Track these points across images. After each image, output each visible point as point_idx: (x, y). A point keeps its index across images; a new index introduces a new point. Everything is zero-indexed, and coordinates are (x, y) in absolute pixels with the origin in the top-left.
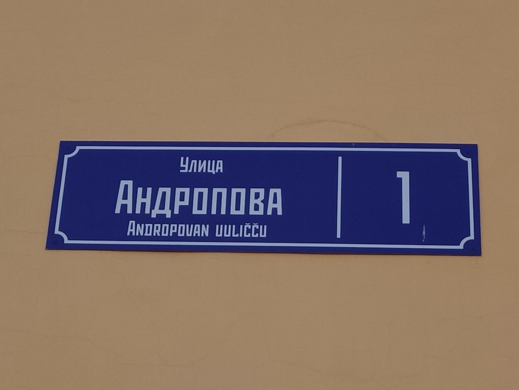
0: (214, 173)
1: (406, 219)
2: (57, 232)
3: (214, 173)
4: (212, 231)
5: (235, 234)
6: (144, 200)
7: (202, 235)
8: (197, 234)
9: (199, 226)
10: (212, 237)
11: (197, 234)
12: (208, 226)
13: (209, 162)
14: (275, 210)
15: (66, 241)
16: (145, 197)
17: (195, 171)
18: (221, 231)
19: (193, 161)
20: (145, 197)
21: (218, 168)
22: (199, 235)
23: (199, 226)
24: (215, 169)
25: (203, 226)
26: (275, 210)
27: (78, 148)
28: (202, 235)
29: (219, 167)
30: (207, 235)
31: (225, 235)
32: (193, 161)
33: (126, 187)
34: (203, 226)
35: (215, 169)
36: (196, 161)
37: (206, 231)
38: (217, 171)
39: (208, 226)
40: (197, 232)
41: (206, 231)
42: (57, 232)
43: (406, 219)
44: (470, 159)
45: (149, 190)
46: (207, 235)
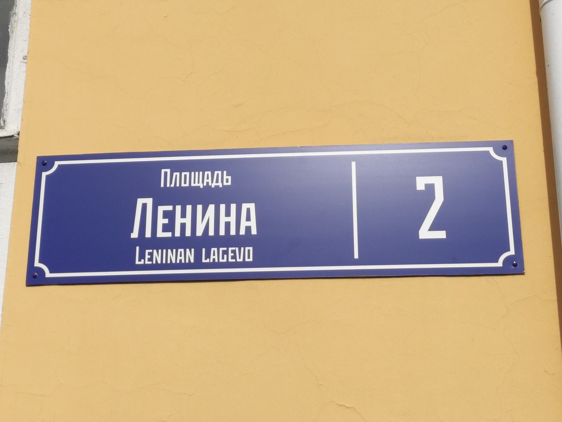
0: (202, 187)
1: (138, 248)
2: (37, 264)
3: (202, 187)
4: (198, 256)
5: (206, 259)
6: (183, 220)
7: (187, 261)
8: (181, 260)
9: (182, 250)
10: (198, 264)
11: (181, 260)
12: (193, 250)
13: (197, 173)
14: (248, 229)
15: (48, 275)
16: (185, 217)
17: (178, 185)
18: (216, 254)
19: (175, 174)
20: (185, 217)
21: (206, 181)
22: (183, 261)
23: (182, 250)
24: (203, 182)
25: (188, 250)
26: (248, 229)
27: (57, 164)
28: (187, 261)
29: (227, 180)
30: (192, 261)
31: (247, 260)
32: (175, 174)
33: (144, 206)
34: (188, 250)
35: (203, 182)
36: (220, 172)
37: (190, 256)
38: (205, 184)
39: (193, 250)
40: (181, 258)
41: (190, 256)
42: (37, 264)
43: (138, 248)
44: (505, 159)
45: (233, 207)
46: (192, 261)
